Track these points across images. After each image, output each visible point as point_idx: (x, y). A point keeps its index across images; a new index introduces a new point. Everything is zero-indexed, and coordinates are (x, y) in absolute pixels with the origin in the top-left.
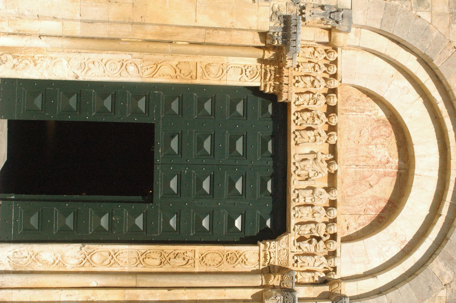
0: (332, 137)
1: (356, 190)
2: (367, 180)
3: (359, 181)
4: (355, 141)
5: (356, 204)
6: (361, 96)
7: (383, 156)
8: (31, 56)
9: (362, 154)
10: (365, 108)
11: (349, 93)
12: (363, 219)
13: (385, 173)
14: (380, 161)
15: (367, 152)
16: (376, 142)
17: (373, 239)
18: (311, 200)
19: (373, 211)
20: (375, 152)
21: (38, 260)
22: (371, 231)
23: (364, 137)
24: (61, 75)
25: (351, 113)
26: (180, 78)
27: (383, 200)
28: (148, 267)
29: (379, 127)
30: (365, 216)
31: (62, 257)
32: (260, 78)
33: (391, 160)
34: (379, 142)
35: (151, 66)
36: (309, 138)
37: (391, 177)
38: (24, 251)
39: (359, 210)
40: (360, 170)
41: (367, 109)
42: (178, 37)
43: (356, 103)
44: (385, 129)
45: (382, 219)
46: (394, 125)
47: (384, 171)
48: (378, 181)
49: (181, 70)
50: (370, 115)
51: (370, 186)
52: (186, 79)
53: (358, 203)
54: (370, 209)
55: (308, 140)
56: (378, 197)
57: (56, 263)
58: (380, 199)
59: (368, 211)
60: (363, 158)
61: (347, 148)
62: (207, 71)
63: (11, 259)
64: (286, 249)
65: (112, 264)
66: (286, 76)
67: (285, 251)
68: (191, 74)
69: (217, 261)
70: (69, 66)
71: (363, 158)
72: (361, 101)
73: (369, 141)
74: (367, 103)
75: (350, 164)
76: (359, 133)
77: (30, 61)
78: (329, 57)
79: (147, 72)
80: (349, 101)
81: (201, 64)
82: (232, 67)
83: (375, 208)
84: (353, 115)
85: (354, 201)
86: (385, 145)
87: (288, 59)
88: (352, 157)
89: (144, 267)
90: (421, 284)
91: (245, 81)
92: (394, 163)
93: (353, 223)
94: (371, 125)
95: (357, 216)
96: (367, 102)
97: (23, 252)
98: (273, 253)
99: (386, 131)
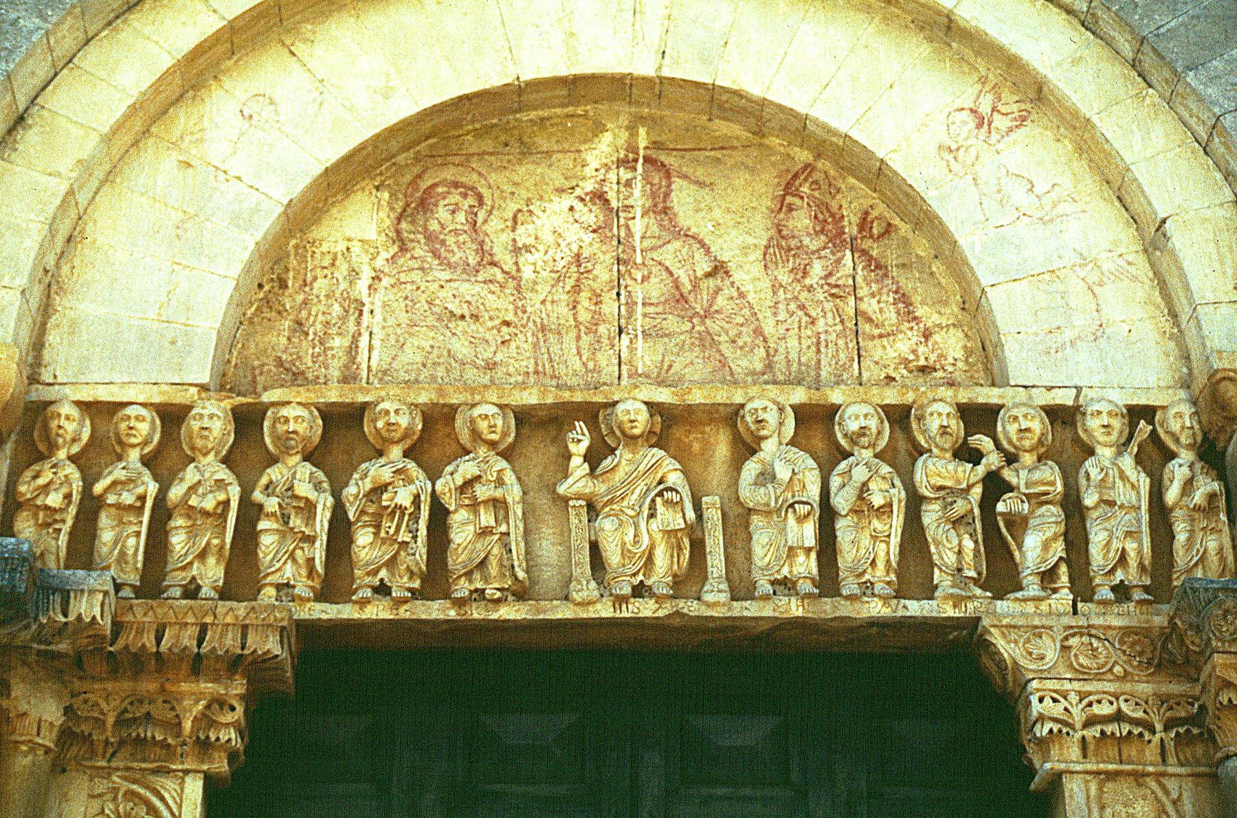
0: (483, 425)
1: (739, 335)
2: (690, 288)
4: (500, 340)
5: (809, 333)
6: (279, 313)
7: (572, 220)
9: (564, 310)
10: (338, 295)
11: (263, 365)
12: (879, 302)
13: (654, 212)
14: (594, 231)
15: (553, 286)
16: (506, 249)
18: (801, 520)
19: (839, 261)
20: (551, 252)
22: (934, 269)
23: (481, 301)
25: (362, 358)
27: (782, 216)
29: (430, 237)
30: (860, 293)
33: (589, 186)
34: (506, 237)
36: (485, 532)
37: (673, 187)
39: (838, 320)
41: (342, 288)
43: (315, 334)
44: (440, 209)
45: (872, 222)
46: (424, 172)
48: (693, 237)
50: (374, 274)
51: (721, 274)
53: (803, 324)
55: (496, 537)
56: (772, 238)
58: (780, 231)
59: (840, 282)
61: (536, 372)
64: (1066, 638)
66: (159, 640)
67: (1073, 641)
73: (500, 277)
78: (74, 440)
80: (303, 368)
83: (823, 253)
84: (371, 349)
85: (793, 343)
86: (520, 211)
87: (66, 616)
88: (579, 353)
90: (1182, 24)
92: (603, 171)
93: (899, 345)
94: (422, 269)
95: (866, 327)
96: (307, 289)
98: (1090, 704)
99: (451, 208)
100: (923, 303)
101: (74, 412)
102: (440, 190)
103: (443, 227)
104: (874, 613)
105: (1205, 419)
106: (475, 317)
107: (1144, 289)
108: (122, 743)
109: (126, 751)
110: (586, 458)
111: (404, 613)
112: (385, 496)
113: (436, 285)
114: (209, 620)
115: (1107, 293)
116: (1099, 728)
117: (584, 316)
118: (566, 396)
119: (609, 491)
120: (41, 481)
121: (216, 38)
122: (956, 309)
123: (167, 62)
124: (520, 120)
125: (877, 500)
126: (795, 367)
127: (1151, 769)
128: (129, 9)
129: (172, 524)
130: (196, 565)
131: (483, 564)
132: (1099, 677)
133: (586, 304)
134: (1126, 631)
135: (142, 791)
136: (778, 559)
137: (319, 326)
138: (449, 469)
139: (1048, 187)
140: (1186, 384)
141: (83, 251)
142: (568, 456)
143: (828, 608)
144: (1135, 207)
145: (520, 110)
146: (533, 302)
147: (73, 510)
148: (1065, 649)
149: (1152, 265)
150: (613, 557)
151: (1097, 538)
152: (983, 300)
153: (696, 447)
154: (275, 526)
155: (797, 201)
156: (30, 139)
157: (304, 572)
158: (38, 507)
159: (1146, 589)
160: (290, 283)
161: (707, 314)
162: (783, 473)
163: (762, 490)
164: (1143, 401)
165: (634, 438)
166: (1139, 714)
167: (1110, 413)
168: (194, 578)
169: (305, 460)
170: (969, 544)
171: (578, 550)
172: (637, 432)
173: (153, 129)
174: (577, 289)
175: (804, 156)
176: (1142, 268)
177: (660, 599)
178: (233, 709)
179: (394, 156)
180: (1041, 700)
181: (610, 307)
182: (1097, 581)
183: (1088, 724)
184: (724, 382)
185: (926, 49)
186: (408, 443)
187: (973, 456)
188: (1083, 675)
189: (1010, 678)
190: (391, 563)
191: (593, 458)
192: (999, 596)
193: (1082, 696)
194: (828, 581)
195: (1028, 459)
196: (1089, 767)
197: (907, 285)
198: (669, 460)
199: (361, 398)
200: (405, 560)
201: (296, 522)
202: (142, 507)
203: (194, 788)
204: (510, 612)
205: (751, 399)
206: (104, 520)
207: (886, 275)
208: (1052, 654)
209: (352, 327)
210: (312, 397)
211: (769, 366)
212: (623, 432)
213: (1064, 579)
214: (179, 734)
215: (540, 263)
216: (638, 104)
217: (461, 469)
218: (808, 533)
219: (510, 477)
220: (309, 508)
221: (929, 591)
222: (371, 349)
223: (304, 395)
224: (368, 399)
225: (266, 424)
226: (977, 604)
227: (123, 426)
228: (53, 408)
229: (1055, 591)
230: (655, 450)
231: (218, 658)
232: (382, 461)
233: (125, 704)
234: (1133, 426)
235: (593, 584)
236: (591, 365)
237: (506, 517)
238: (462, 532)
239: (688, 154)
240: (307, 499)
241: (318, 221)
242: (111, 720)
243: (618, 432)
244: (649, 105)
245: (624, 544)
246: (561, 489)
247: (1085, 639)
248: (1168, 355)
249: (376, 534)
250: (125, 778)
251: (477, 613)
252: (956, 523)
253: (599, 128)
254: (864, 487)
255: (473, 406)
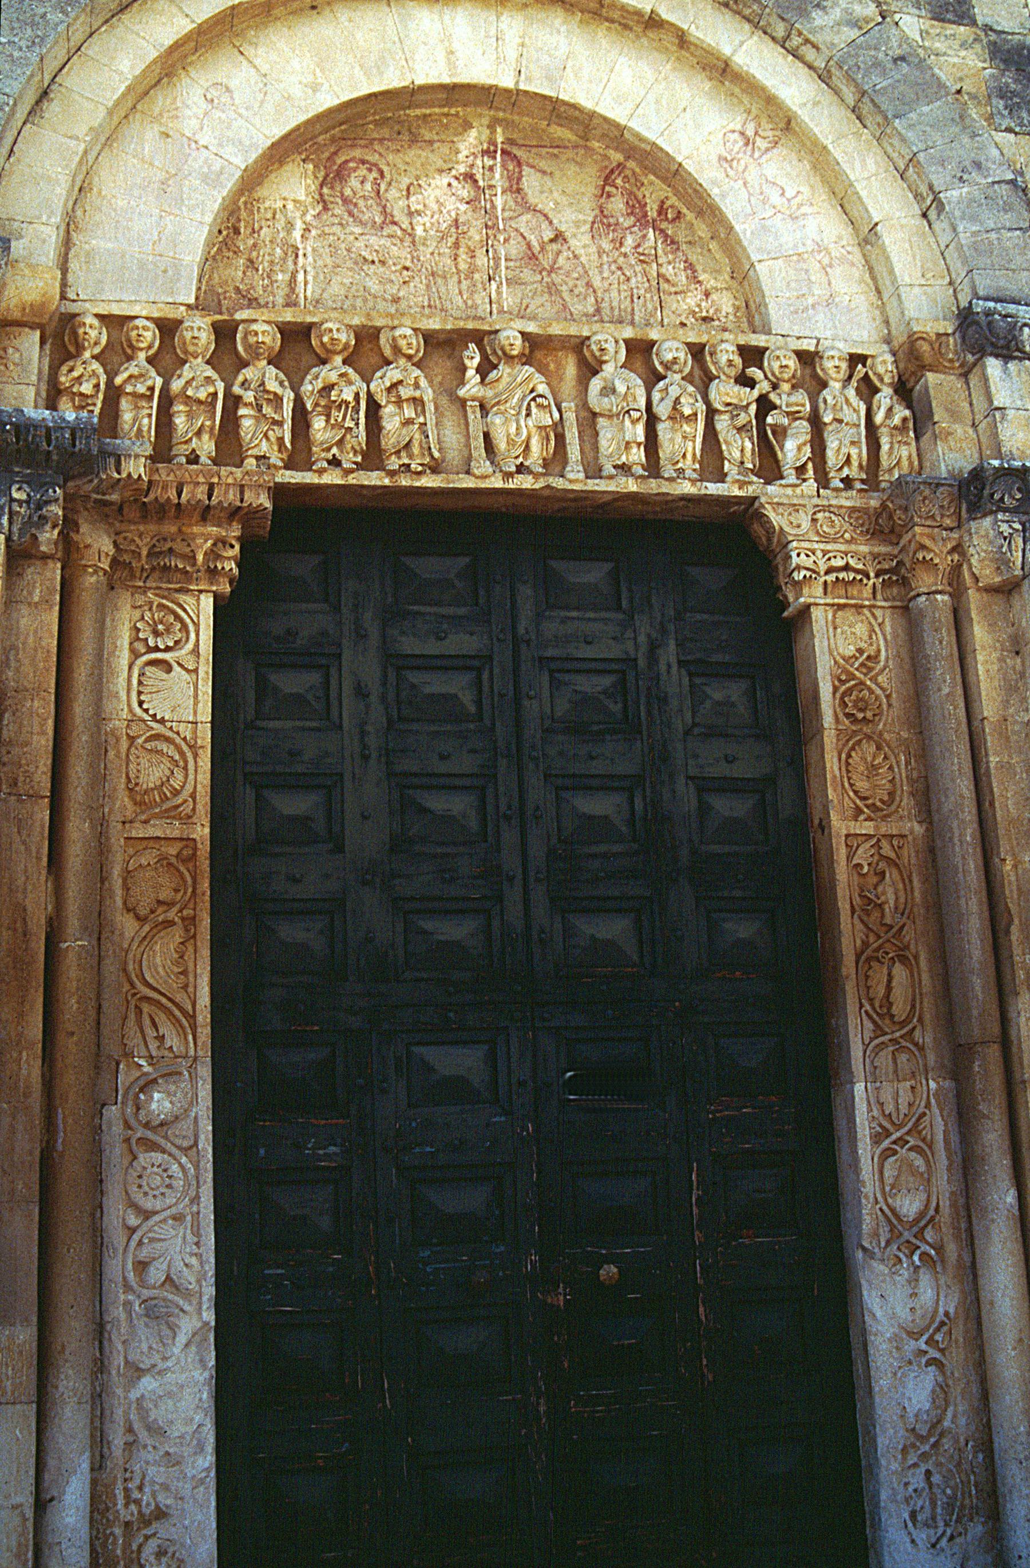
0: (402, 343)
3: (544, 273)
8: (124, 1536)
17: (748, 233)
18: (634, 422)
19: (644, 236)
20: (436, 217)
21: (933, 1426)
24: (200, 1400)
25: (300, 288)
26: (191, 905)
27: (603, 200)
28: (921, 1008)
29: (346, 201)
30: (660, 261)
31: (914, 1335)
32: (182, 598)
33: (462, 169)
35: (147, 1022)
36: (409, 422)
38: (906, 1484)
40: (503, 268)
42: (29, 908)
47: (504, 192)
49: (159, 902)
51: (560, 240)
52: (195, 882)
54: (639, 245)
56: (596, 216)
57: (937, 1355)
60: (463, 256)
61: (430, 306)
62: (158, 799)
63: (940, 1531)
65: (924, 1140)
67: (819, 516)
68: (173, 860)
69: (874, 758)
70: (161, 1366)
71: (463, 256)
72: (254, 254)
73: (399, 233)
74: (262, 233)
75: (487, 300)
76: (373, 267)
77: (147, 1538)
78: (96, 344)
79: (173, 1040)
81: (131, 822)
82: (140, 693)
84: (306, 283)
87: (119, 473)
88: (460, 293)
89: (920, 1020)
91: (196, 651)
93: (688, 300)
95: (664, 286)
97: (910, 1489)
100: (704, 271)
101: (96, 322)
102: (352, 165)
103: (355, 193)
104: (686, 491)
105: (902, 366)
106: (383, 263)
107: (859, 271)
108: (153, 569)
109: (156, 574)
110: (478, 371)
111: (352, 480)
112: (333, 393)
113: (352, 238)
114: (215, 480)
115: (836, 273)
116: (835, 575)
117: (463, 266)
118: (461, 324)
119: (496, 396)
120: (76, 374)
121: (187, 38)
122: (727, 278)
123: (154, 54)
124: (408, 115)
125: (687, 411)
126: (616, 313)
127: (867, 603)
128: (121, 10)
129: (175, 409)
130: (194, 440)
131: (408, 446)
132: (835, 541)
133: (464, 257)
134: (853, 510)
135: (170, 604)
136: (619, 448)
137: (266, 264)
138: (378, 374)
139: (794, 194)
140: (888, 341)
141: (92, 197)
142: (464, 369)
143: (653, 486)
144: (854, 214)
145: (409, 108)
146: (425, 253)
147: (101, 396)
148: (814, 520)
149: (864, 255)
150: (501, 445)
151: (832, 445)
152: (751, 273)
153: (552, 366)
154: (252, 413)
155: (613, 190)
156: (53, 109)
157: (276, 448)
158: (74, 394)
159: (863, 481)
160: (242, 230)
161: (552, 270)
162: (621, 389)
163: (606, 399)
164: (860, 351)
165: (512, 357)
166: (860, 566)
167: (839, 359)
168: (194, 450)
169: (269, 363)
170: (748, 445)
171: (476, 439)
172: (515, 353)
173: (139, 107)
174: (456, 245)
175: (617, 157)
176: (857, 257)
177: (537, 476)
178: (232, 546)
179: (316, 137)
180: (798, 555)
181: (481, 260)
182: (831, 475)
183: (827, 573)
184: (566, 319)
185: (707, 85)
186: (346, 354)
187: (749, 383)
188: (825, 539)
189: (775, 540)
190: (340, 443)
191: (484, 370)
192: (768, 482)
193: (825, 553)
194: (653, 466)
195: (786, 387)
196: (829, 601)
197: (693, 258)
198: (537, 375)
199: (309, 319)
200: (350, 441)
201: (267, 410)
202: (152, 395)
203: (207, 603)
204: (429, 481)
205: (595, 333)
206: (124, 404)
207: (678, 249)
208: (806, 524)
209: (291, 267)
210: (273, 317)
211: (598, 310)
212: (505, 353)
213: (810, 472)
214: (194, 564)
215: (428, 225)
216: (498, 109)
217: (388, 374)
218: (640, 432)
219: (423, 383)
220: (277, 401)
221: (721, 477)
222: (306, 283)
223: (264, 315)
224: (315, 320)
225: (238, 336)
226: (755, 487)
227: (134, 333)
228: (78, 318)
229: (804, 480)
230: (527, 367)
231: (223, 509)
232: (328, 367)
233: (154, 541)
234: (852, 368)
235: (488, 463)
236: (470, 303)
237: (424, 412)
238: (391, 421)
239: (534, 150)
240: (275, 394)
241: (260, 184)
242: (144, 553)
243: (500, 353)
244: (504, 111)
245: (508, 435)
246: (462, 393)
247: (827, 514)
248: (874, 319)
249: (327, 421)
250: (156, 595)
251: (405, 481)
252: (739, 430)
253: (467, 126)
254: (677, 401)
255: (394, 328)
